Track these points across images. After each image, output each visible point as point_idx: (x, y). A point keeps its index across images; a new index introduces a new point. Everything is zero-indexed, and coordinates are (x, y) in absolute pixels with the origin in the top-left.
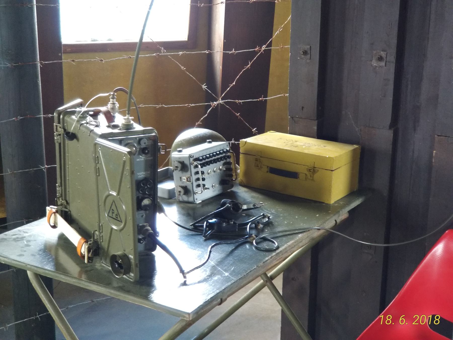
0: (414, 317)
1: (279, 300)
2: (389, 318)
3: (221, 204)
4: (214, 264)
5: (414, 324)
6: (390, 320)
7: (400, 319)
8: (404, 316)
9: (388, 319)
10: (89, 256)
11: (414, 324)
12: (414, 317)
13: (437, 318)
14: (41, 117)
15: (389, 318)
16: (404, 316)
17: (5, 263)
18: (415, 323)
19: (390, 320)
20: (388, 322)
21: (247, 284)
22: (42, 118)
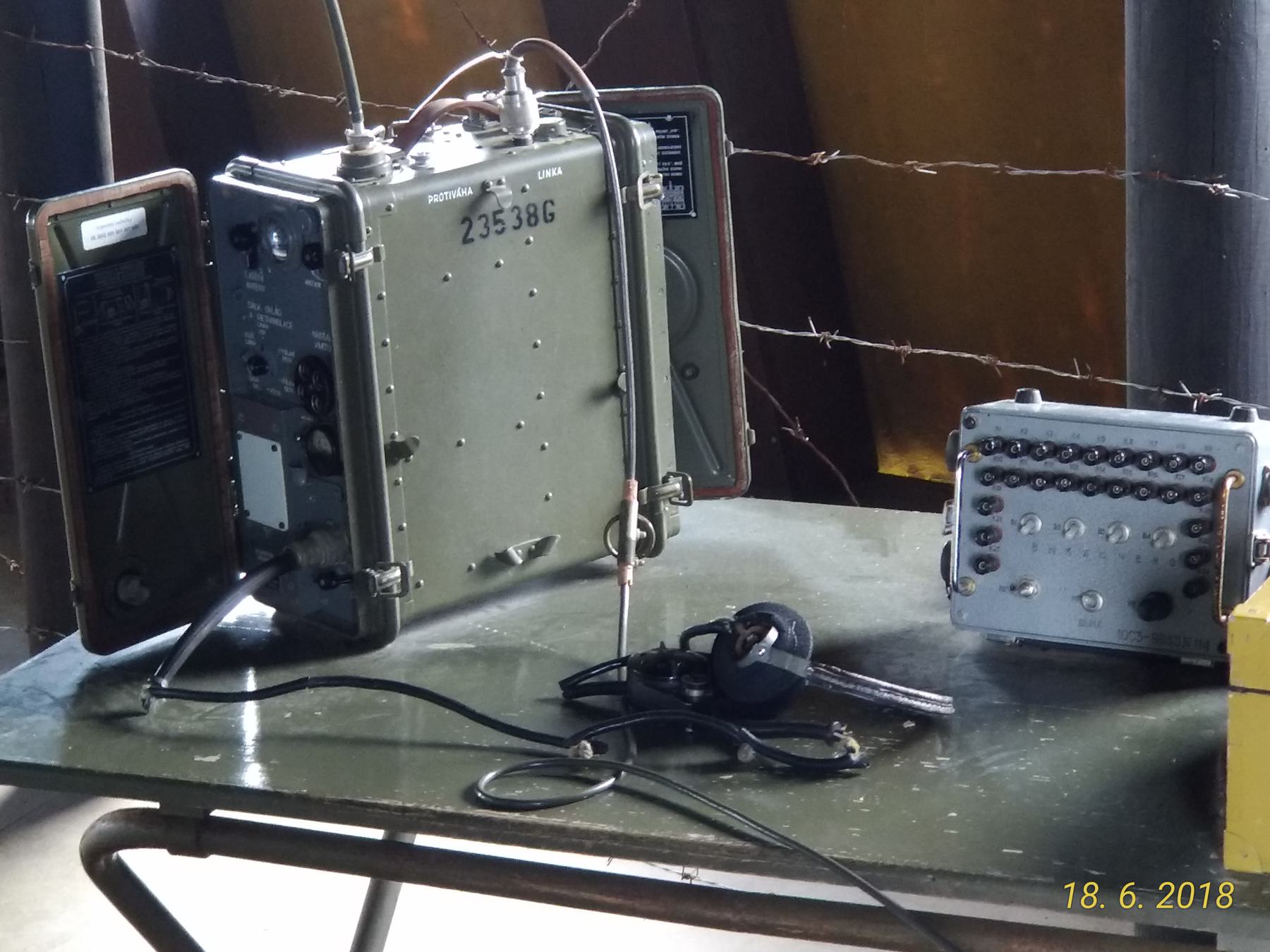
0: (1161, 888)
1: (853, 931)
2: (1226, 889)
3: (735, 774)
4: (381, 162)
5: (1159, 906)
6: (1228, 895)
7: (1123, 894)
8: (1133, 884)
9: (1223, 895)
10: (747, 747)
11: (1159, 906)
12: (1161, 888)
13: (1226, 889)
14: (12, 338)
15: (1091, 889)
16: (1133, 884)
17: (543, 537)
18: (1163, 904)
19: (1228, 895)
20: (1089, 901)
21: (892, 868)
22: (4, 337)
